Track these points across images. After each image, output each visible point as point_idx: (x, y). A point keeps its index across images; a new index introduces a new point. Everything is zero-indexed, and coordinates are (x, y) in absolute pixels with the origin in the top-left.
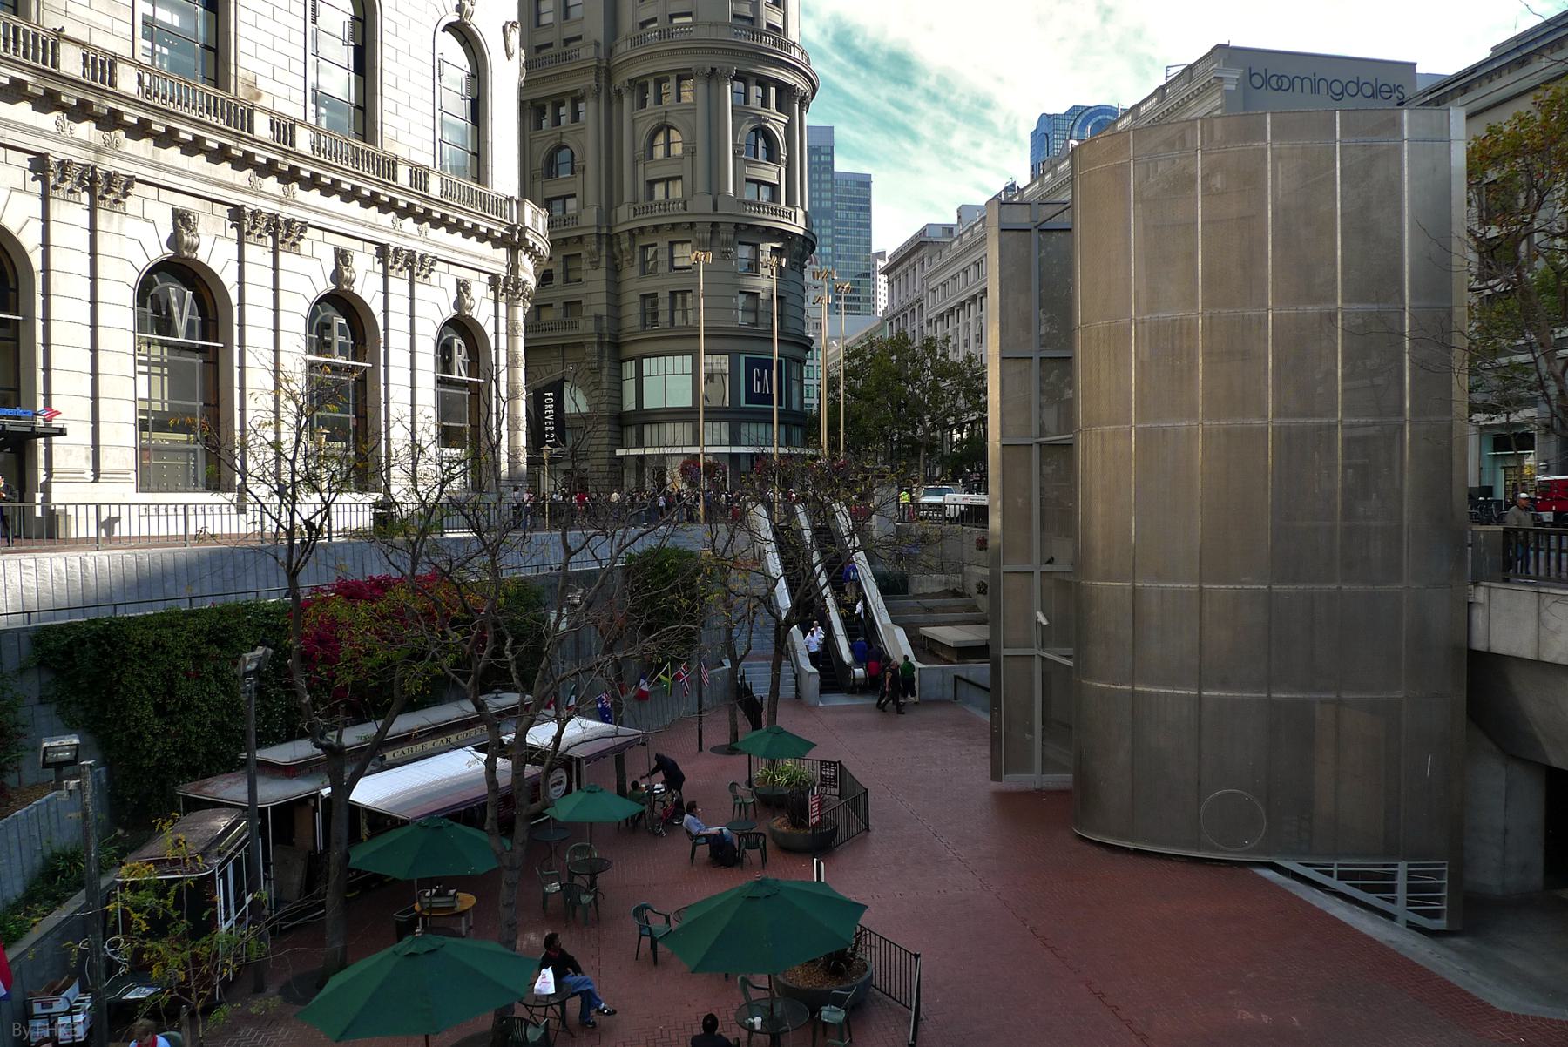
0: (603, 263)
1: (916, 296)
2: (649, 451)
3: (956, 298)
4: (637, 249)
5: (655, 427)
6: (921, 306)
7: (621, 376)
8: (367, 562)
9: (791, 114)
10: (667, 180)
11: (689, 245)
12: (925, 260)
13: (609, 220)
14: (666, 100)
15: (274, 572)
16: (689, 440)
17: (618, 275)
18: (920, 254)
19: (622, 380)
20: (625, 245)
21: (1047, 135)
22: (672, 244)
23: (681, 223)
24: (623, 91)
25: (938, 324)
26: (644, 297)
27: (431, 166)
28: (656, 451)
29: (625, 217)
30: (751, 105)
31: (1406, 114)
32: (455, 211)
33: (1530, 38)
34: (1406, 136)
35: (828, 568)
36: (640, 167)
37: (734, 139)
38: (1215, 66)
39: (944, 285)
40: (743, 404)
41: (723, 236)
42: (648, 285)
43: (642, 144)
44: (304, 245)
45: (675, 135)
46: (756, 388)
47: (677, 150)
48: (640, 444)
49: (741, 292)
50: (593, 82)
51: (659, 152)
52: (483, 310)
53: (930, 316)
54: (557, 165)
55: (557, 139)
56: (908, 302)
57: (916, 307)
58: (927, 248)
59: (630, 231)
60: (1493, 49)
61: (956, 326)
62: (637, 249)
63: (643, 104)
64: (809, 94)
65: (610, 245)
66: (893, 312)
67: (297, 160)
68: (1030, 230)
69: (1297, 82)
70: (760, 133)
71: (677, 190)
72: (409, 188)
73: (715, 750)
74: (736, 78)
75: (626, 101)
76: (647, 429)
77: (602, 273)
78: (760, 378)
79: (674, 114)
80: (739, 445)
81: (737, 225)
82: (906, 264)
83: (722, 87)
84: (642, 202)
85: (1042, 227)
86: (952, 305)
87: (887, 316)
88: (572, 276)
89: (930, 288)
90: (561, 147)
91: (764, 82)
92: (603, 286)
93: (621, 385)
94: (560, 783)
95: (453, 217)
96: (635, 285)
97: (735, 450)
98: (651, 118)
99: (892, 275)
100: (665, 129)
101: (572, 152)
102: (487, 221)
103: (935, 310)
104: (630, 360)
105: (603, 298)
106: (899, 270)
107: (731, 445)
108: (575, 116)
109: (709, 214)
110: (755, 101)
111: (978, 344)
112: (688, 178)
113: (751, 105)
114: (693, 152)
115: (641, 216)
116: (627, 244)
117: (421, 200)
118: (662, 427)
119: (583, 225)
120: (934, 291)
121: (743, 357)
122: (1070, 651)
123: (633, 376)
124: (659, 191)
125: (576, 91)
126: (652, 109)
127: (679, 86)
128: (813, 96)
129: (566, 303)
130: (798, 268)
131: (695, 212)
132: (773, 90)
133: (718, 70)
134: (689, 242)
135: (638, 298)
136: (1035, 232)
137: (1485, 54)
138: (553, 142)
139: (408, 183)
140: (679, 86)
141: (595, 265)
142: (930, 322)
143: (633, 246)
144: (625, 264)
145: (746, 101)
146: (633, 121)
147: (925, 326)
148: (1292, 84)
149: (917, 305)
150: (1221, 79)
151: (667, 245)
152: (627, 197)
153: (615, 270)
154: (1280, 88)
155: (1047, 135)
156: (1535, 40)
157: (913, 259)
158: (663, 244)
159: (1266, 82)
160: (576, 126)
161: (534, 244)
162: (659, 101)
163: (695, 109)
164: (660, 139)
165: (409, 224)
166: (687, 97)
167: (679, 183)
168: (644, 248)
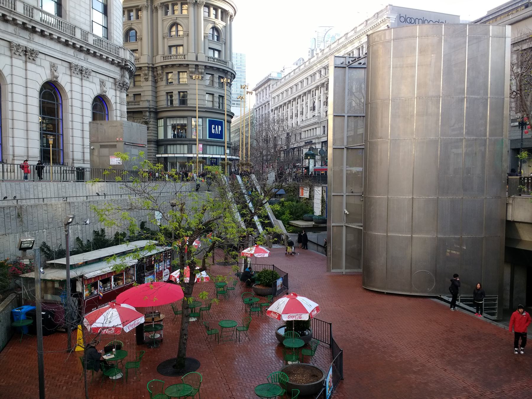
0: (150, 78)
1: (266, 100)
2: (170, 155)
3: (283, 101)
4: (164, 74)
5: (172, 146)
6: (269, 104)
7: (157, 125)
8: (78, 191)
9: (226, 22)
10: (177, 46)
11: (186, 73)
12: (271, 86)
13: (152, 61)
14: (176, 13)
15: (41, 193)
16: (186, 151)
17: (156, 84)
18: (269, 83)
19: (158, 127)
20: (160, 72)
21: (315, 39)
22: (179, 72)
23: (183, 64)
24: (158, 7)
25: (276, 111)
26: (167, 93)
27: (89, 32)
28: (173, 155)
29: (159, 60)
30: (211, 17)
31: (491, 27)
32: (99, 51)
33: (502, 8)
34: (491, 35)
35: (252, 200)
36: (166, 40)
37: (204, 30)
38: (387, 13)
39: (278, 96)
40: (208, 138)
41: (200, 70)
42: (169, 88)
43: (166, 30)
44: (38, 61)
45: (180, 28)
46: (213, 131)
47: (181, 33)
48: (166, 152)
49: (207, 93)
50: (146, 3)
51: (173, 33)
52: (111, 94)
53: (272, 108)
54: (130, 37)
55: (130, 26)
56: (263, 102)
57: (267, 104)
58: (272, 81)
59: (162, 66)
60: (488, 12)
61: (287, 110)
62: (164, 74)
63: (166, 13)
64: (233, 14)
65: (153, 72)
66: (257, 106)
67: (35, 24)
68: (345, 67)
69: (417, 20)
70: (214, 29)
71: (180, 50)
72: (81, 40)
73: (219, 264)
74: (205, 6)
75: (160, 12)
76: (169, 147)
77: (150, 83)
78: (215, 128)
79: (180, 19)
80: (206, 154)
81: (205, 66)
82: (263, 87)
83: (199, 9)
84: (167, 54)
85: (349, 66)
86: (281, 104)
87: (255, 107)
88: (137, 83)
89: (272, 97)
90: (131, 29)
91: (216, 8)
92: (150, 88)
93: (157, 128)
94: (167, 275)
95: (99, 53)
96: (163, 88)
97: (205, 156)
98: (170, 19)
99: (257, 92)
100: (176, 24)
101: (136, 32)
102: (112, 56)
103: (274, 106)
104: (161, 118)
105: (150, 93)
106: (260, 90)
107: (203, 154)
108: (138, 17)
109: (195, 61)
110: (213, 16)
111: (301, 115)
112: (185, 46)
113: (211, 17)
114: (188, 35)
115: (166, 60)
116: (160, 72)
117: (86, 45)
118: (175, 146)
119: (141, 63)
120: (274, 98)
121: (208, 119)
122: (362, 224)
123: (163, 125)
124: (174, 50)
125: (138, 6)
126: (170, 16)
127: (182, 7)
128: (235, 15)
129: (134, 95)
130: (229, 85)
131: (189, 60)
132: (220, 11)
133: (198, 2)
134: (186, 72)
135: (165, 94)
136: (347, 68)
137: (485, 14)
138: (128, 27)
139: (80, 38)
140: (182, 7)
141: (146, 79)
142: (272, 110)
143: (163, 73)
144: (159, 80)
145: (209, 15)
146: (163, 20)
147: (270, 111)
148: (415, 21)
149: (264, 105)
150: (389, 18)
151: (177, 73)
152: (160, 52)
153: (155, 82)
154: (411, 23)
155: (315, 39)
156: (504, 9)
157: (266, 85)
158: (175, 72)
159: (406, 20)
160: (138, 21)
161: (131, 67)
162: (173, 13)
163: (189, 17)
164: (174, 29)
165: (82, 56)
166: (185, 12)
167: (181, 48)
168: (168, 73)
